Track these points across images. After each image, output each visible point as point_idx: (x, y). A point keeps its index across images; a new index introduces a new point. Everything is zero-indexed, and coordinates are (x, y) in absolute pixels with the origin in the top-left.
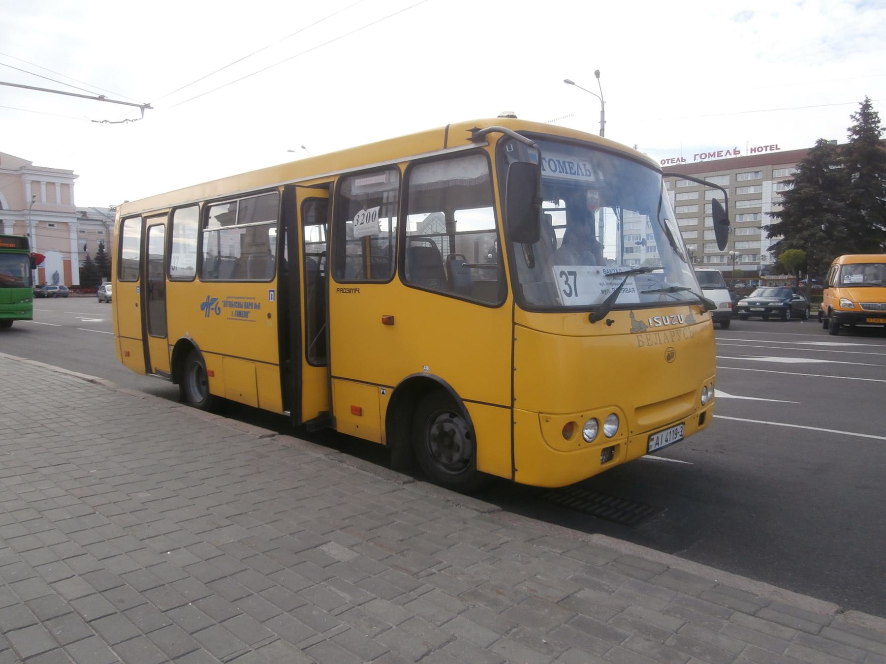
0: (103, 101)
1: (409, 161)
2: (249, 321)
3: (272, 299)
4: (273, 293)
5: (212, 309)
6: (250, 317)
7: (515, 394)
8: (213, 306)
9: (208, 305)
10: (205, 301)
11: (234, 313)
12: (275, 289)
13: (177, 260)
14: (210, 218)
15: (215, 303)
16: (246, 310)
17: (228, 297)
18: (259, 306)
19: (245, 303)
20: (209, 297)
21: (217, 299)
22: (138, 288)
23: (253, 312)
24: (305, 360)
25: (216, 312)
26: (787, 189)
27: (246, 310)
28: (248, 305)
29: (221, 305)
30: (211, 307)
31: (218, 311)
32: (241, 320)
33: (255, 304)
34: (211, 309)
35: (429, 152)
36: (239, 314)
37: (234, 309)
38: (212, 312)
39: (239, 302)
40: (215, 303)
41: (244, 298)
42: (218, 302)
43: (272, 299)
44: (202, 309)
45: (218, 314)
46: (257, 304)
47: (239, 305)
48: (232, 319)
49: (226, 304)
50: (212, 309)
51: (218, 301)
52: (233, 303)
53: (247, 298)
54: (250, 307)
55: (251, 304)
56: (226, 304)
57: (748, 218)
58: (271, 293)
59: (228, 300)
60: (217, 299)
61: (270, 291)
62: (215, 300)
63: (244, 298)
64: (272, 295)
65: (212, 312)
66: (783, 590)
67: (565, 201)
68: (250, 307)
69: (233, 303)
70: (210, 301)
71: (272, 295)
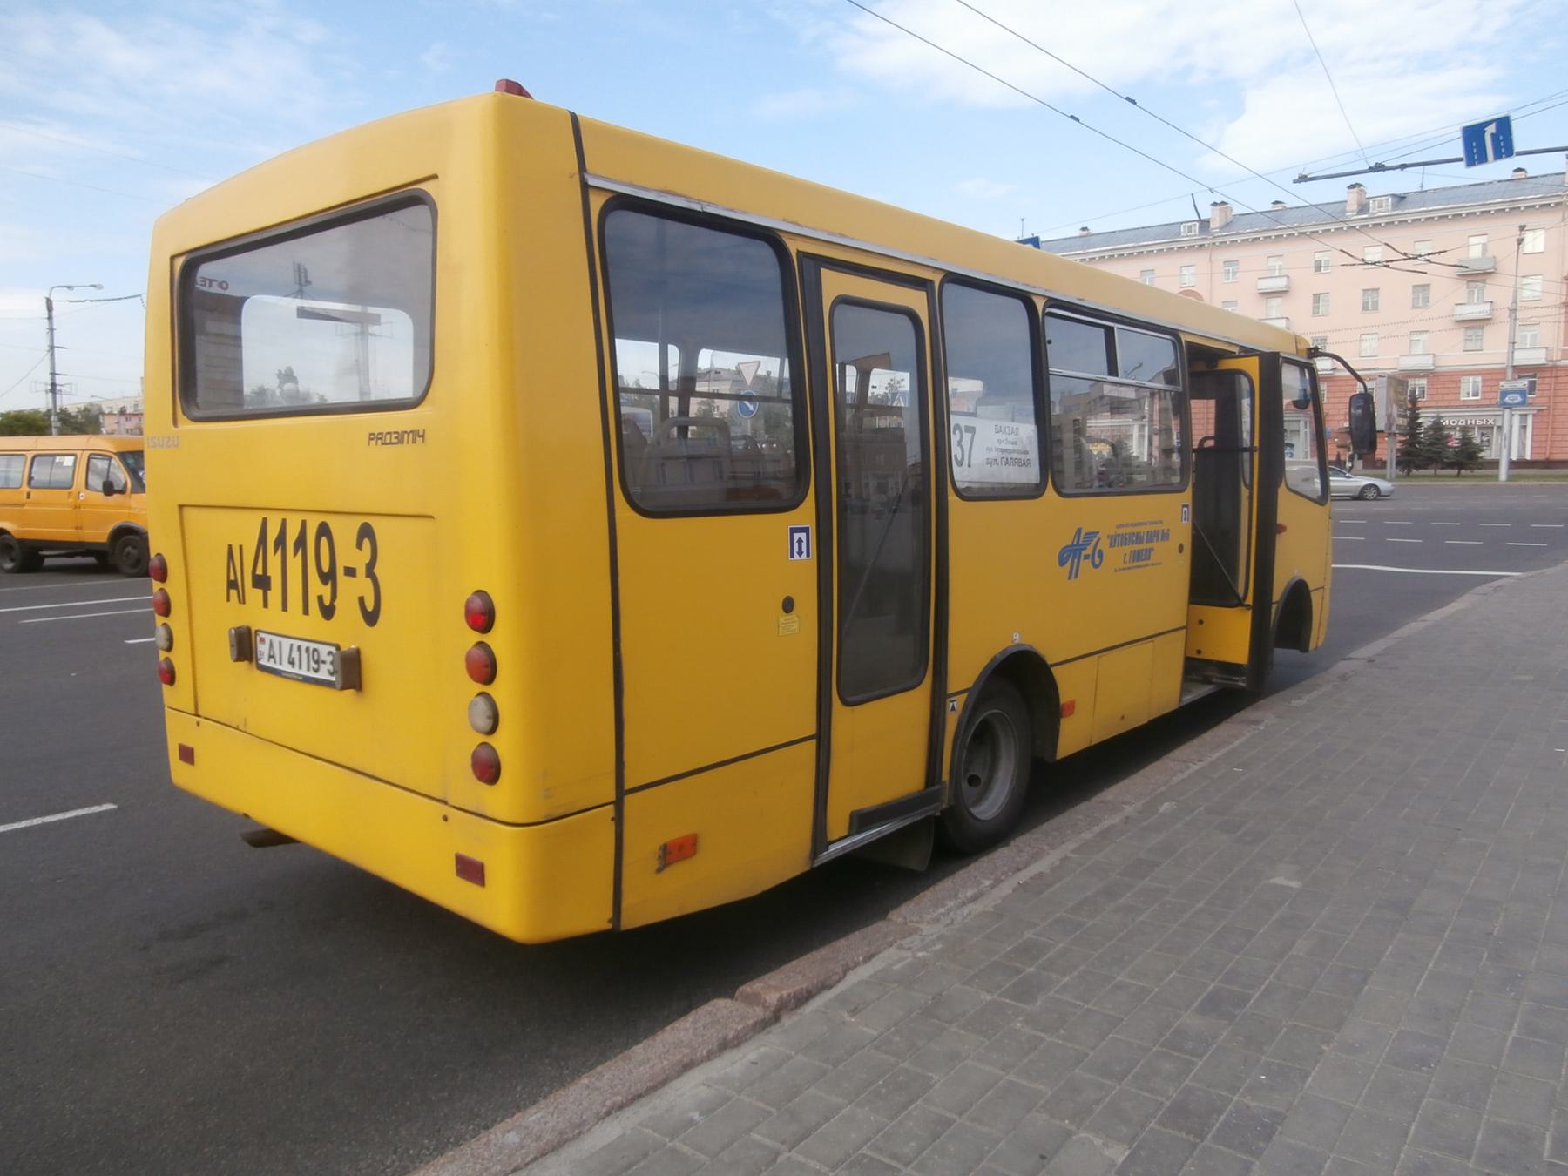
0: (1384, 170)
1: (617, 192)
2: (1153, 565)
3: (800, 553)
4: (803, 536)
5: (1086, 557)
6: (1154, 557)
7: (435, 796)
8: (1089, 551)
9: (1075, 553)
10: (1069, 543)
11: (1128, 557)
12: (1189, 503)
13: (967, 436)
14: (1050, 342)
15: (1093, 543)
16: (1149, 546)
17: (1119, 526)
18: (1168, 534)
19: (1148, 532)
20: (1079, 530)
21: (1098, 533)
22: (1185, 509)
23: (1158, 546)
24: (838, 700)
25: (1093, 562)
26: (1404, 439)
27: (1149, 546)
28: (1152, 536)
29: (1104, 545)
30: (1084, 553)
31: (1097, 559)
32: (1139, 567)
33: (1163, 530)
34: (1082, 557)
35: (631, 185)
36: (1138, 556)
37: (1128, 549)
38: (1085, 565)
39: (1137, 533)
40: (1093, 543)
41: (1145, 524)
42: (1099, 540)
43: (800, 553)
44: (1062, 563)
45: (1096, 566)
46: (1165, 531)
47: (1138, 538)
48: (1124, 569)
49: (1114, 541)
50: (1086, 557)
51: (1098, 536)
52: (1127, 536)
53: (1152, 523)
54: (1155, 539)
55: (1156, 533)
56: (1114, 541)
57: (674, 403)
58: (796, 536)
59: (1118, 532)
60: (1098, 533)
61: (793, 531)
62: (1092, 535)
63: (1145, 524)
64: (800, 541)
65: (1085, 565)
66: (1479, 588)
67: (678, 348)
68: (1155, 539)
69: (1127, 536)
70: (1081, 542)
71: (800, 541)
